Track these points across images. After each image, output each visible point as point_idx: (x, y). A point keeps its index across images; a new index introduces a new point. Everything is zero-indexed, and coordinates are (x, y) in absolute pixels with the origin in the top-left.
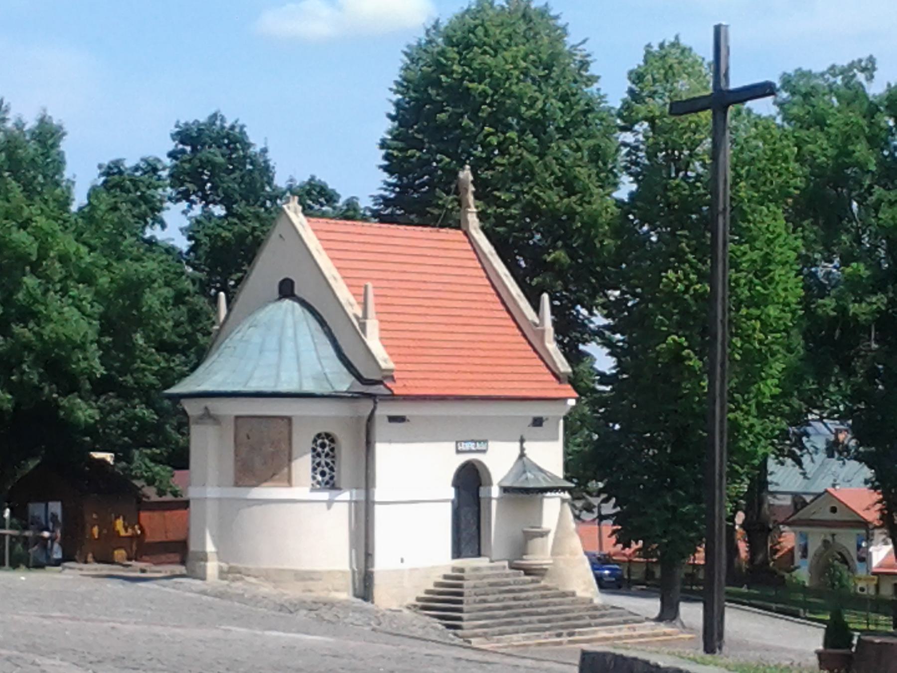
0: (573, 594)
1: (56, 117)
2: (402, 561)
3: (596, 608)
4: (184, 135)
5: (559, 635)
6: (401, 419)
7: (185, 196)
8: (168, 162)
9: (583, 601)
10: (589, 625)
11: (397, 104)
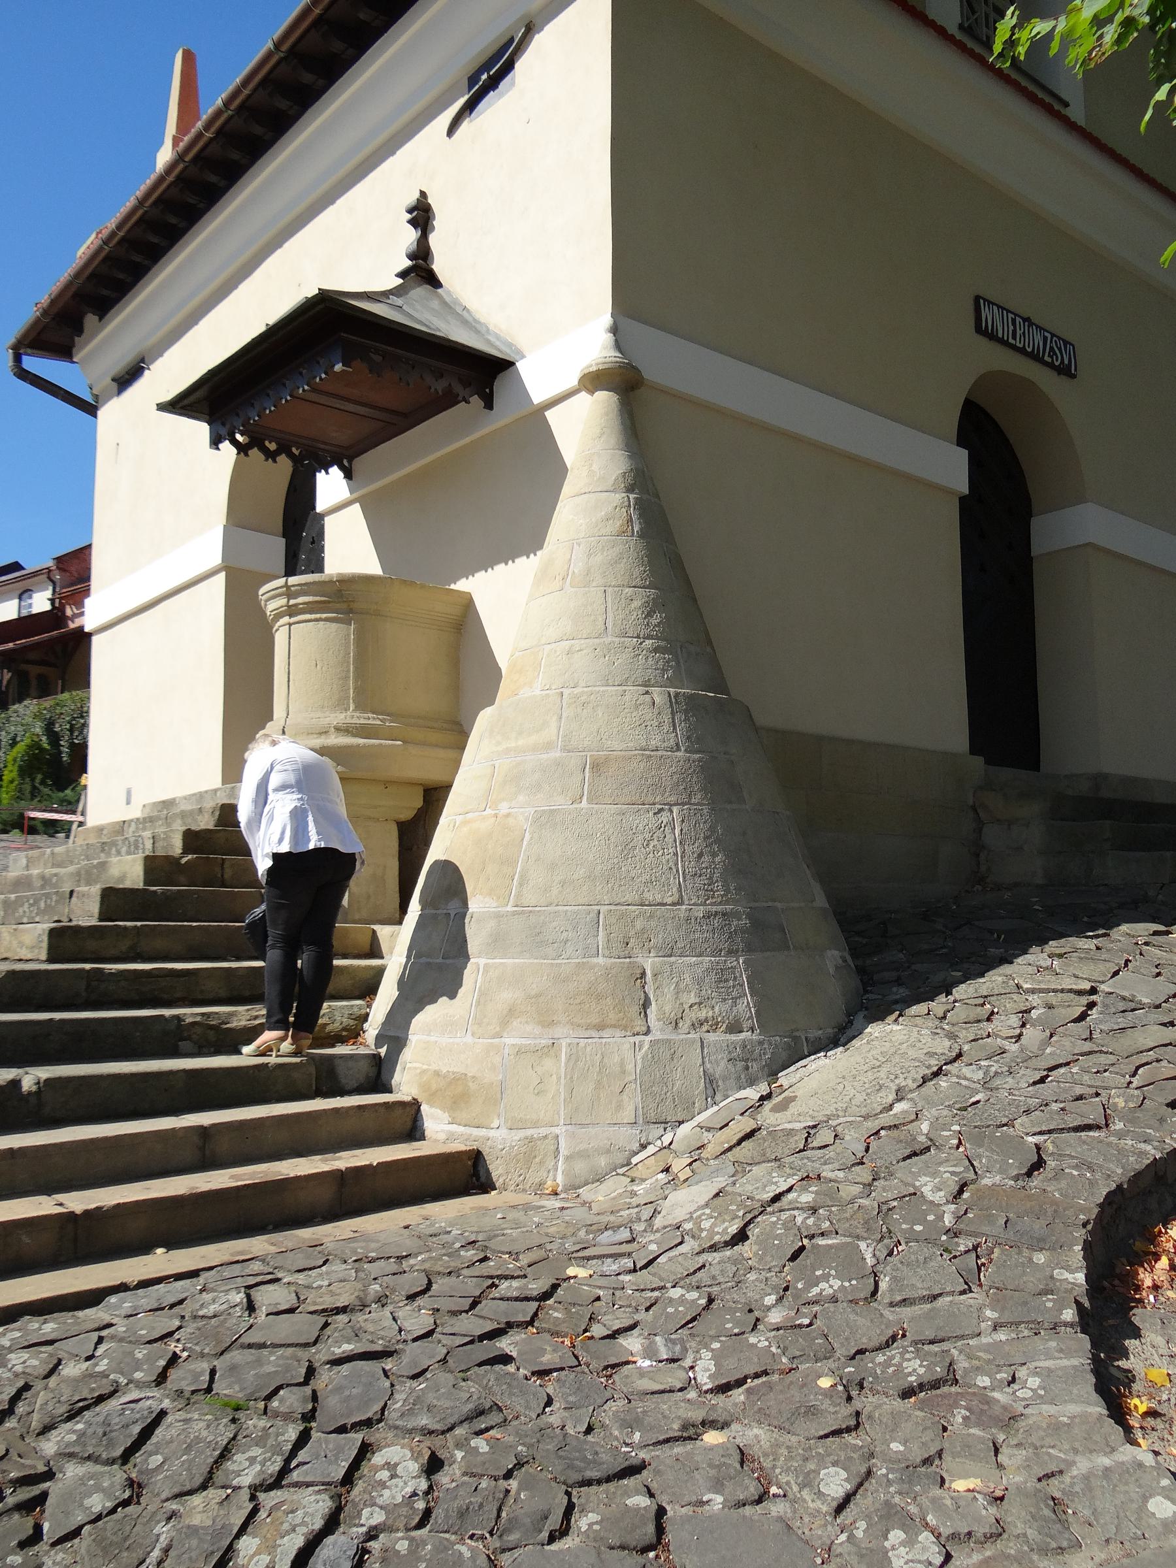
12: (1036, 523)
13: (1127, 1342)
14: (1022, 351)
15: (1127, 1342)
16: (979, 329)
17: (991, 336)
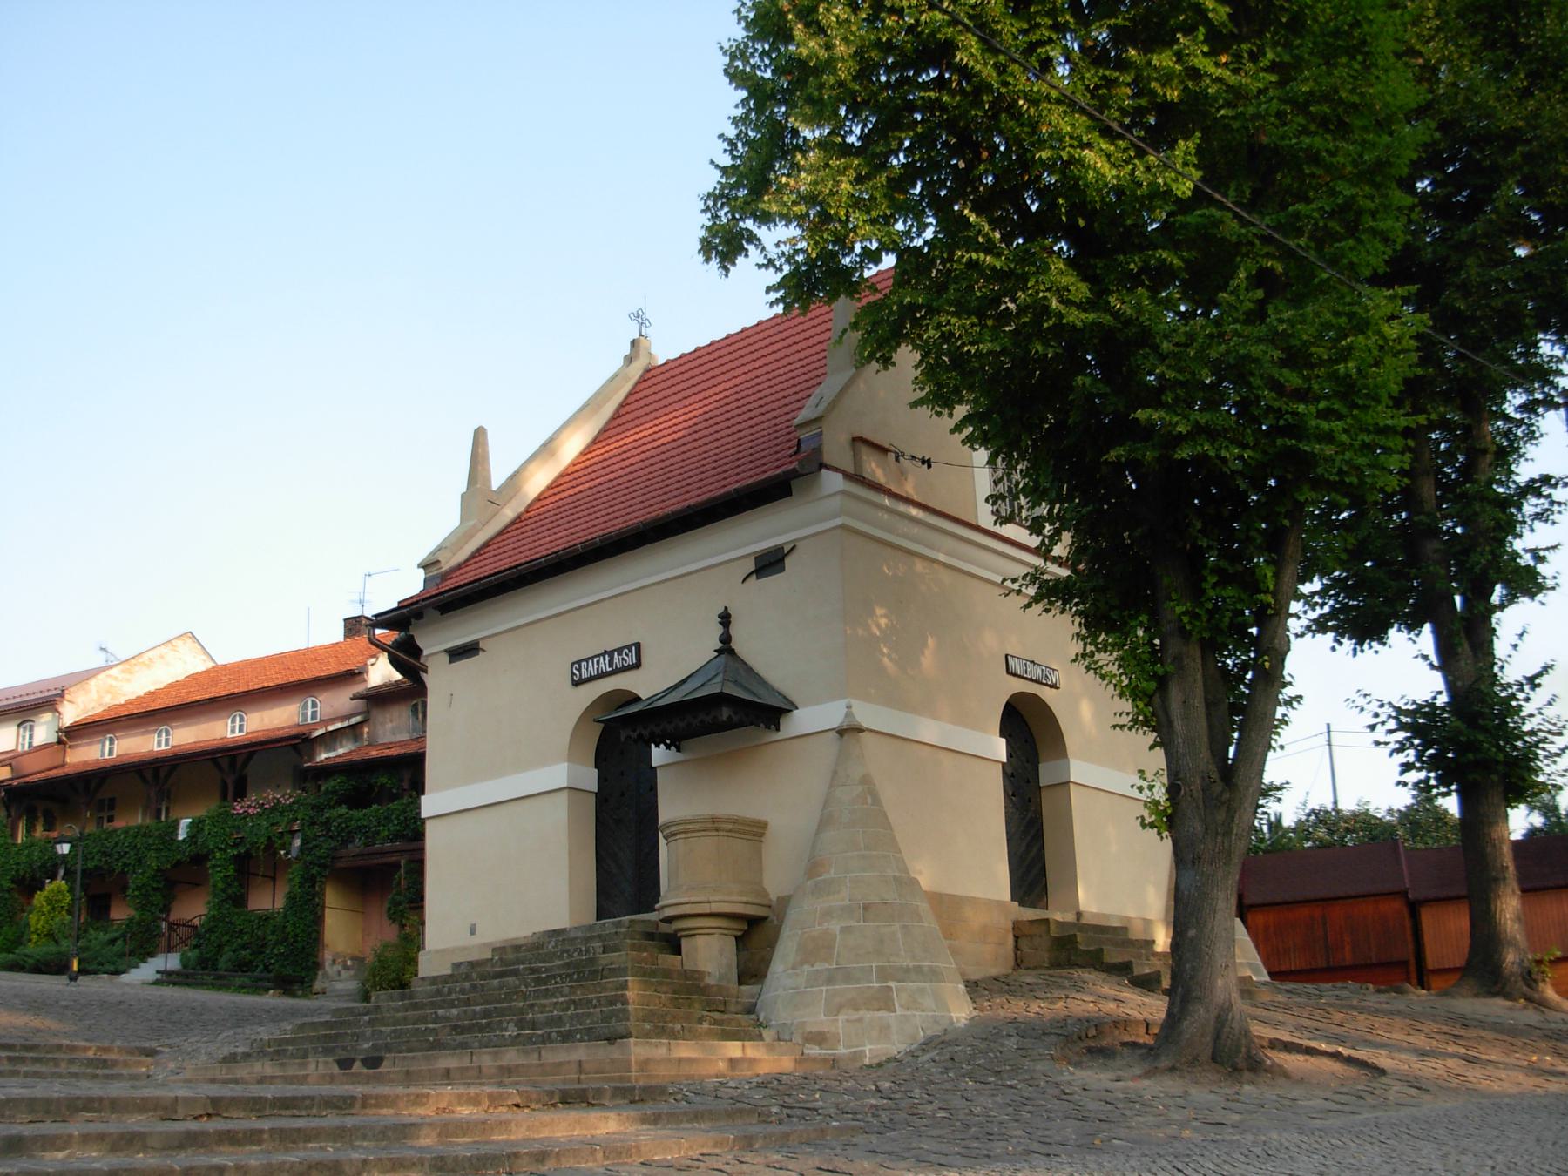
2: (473, 932)
12: (1042, 767)
13: (1427, 627)
14: (1031, 680)
15: (1427, 627)
16: (1008, 672)
17: (1015, 675)
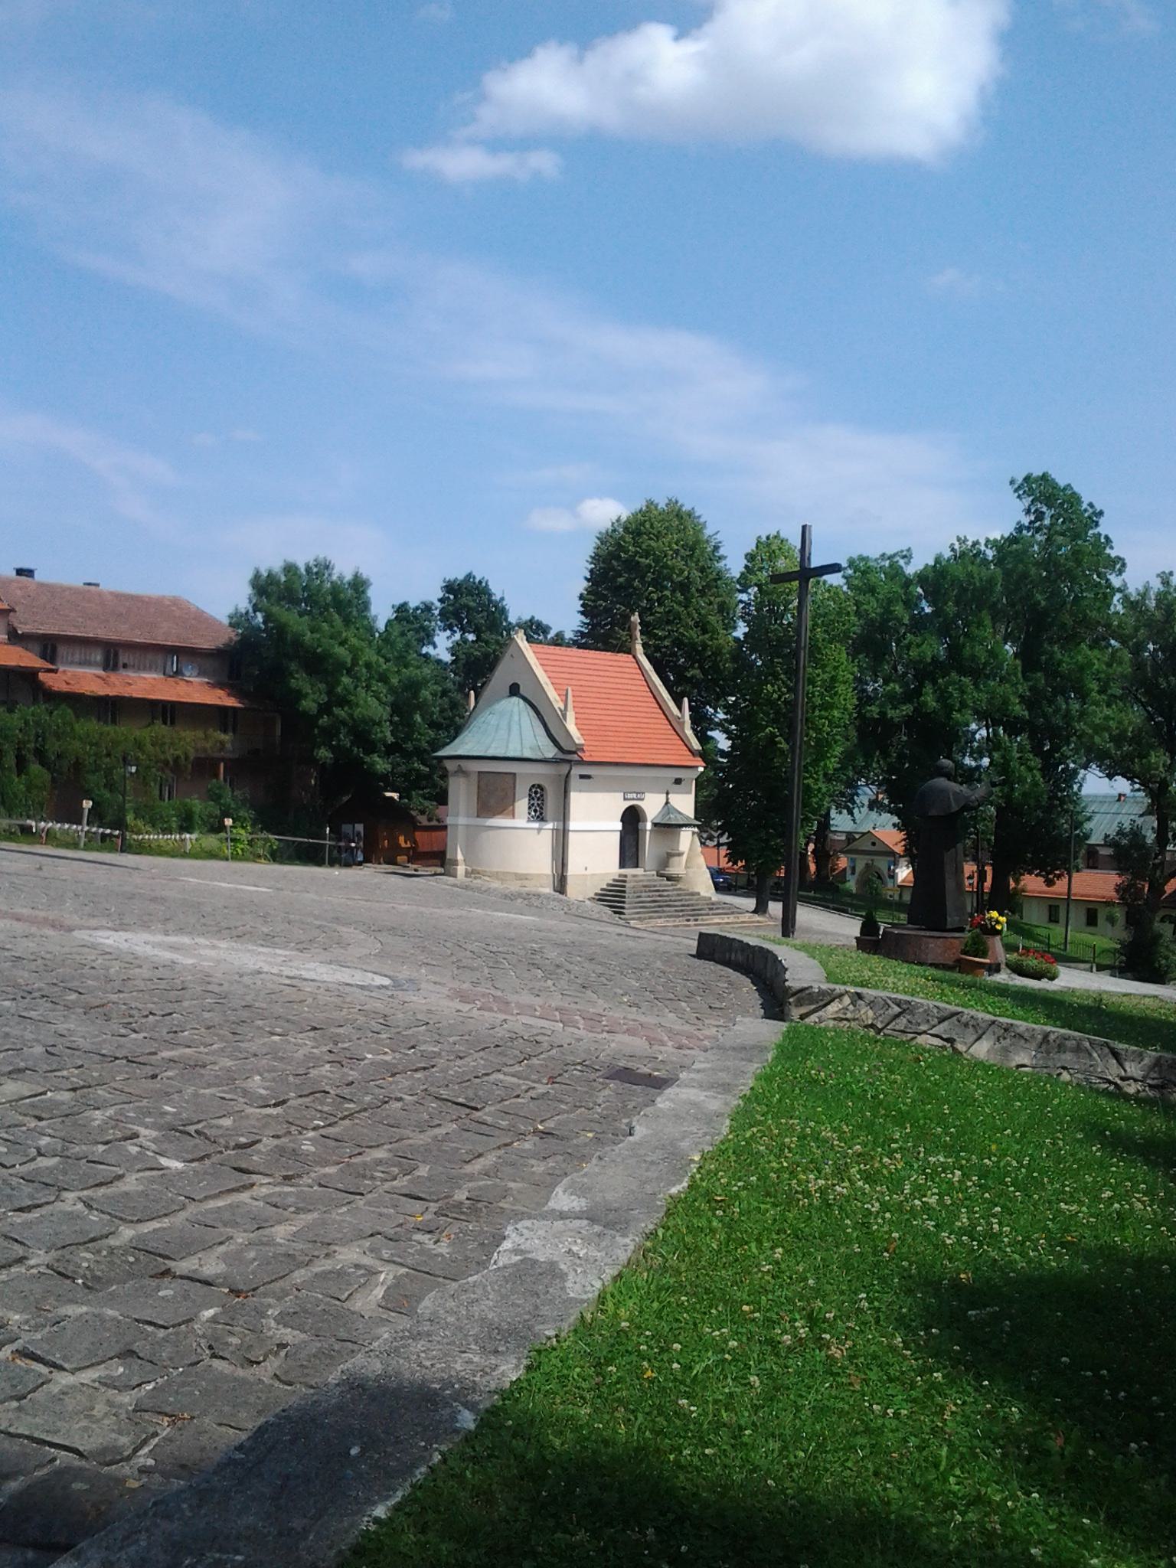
0: (698, 894)
1: (365, 573)
3: (713, 904)
4: (450, 587)
5: (688, 920)
6: (588, 777)
7: (450, 627)
8: (438, 604)
9: (705, 898)
10: (708, 915)
11: (591, 571)
